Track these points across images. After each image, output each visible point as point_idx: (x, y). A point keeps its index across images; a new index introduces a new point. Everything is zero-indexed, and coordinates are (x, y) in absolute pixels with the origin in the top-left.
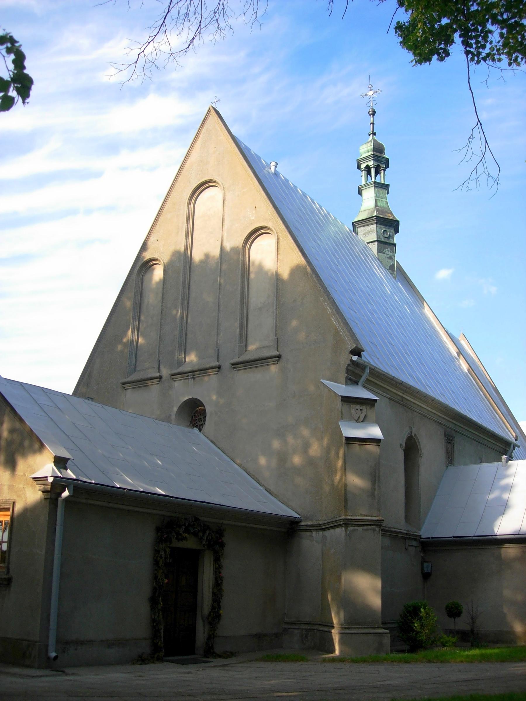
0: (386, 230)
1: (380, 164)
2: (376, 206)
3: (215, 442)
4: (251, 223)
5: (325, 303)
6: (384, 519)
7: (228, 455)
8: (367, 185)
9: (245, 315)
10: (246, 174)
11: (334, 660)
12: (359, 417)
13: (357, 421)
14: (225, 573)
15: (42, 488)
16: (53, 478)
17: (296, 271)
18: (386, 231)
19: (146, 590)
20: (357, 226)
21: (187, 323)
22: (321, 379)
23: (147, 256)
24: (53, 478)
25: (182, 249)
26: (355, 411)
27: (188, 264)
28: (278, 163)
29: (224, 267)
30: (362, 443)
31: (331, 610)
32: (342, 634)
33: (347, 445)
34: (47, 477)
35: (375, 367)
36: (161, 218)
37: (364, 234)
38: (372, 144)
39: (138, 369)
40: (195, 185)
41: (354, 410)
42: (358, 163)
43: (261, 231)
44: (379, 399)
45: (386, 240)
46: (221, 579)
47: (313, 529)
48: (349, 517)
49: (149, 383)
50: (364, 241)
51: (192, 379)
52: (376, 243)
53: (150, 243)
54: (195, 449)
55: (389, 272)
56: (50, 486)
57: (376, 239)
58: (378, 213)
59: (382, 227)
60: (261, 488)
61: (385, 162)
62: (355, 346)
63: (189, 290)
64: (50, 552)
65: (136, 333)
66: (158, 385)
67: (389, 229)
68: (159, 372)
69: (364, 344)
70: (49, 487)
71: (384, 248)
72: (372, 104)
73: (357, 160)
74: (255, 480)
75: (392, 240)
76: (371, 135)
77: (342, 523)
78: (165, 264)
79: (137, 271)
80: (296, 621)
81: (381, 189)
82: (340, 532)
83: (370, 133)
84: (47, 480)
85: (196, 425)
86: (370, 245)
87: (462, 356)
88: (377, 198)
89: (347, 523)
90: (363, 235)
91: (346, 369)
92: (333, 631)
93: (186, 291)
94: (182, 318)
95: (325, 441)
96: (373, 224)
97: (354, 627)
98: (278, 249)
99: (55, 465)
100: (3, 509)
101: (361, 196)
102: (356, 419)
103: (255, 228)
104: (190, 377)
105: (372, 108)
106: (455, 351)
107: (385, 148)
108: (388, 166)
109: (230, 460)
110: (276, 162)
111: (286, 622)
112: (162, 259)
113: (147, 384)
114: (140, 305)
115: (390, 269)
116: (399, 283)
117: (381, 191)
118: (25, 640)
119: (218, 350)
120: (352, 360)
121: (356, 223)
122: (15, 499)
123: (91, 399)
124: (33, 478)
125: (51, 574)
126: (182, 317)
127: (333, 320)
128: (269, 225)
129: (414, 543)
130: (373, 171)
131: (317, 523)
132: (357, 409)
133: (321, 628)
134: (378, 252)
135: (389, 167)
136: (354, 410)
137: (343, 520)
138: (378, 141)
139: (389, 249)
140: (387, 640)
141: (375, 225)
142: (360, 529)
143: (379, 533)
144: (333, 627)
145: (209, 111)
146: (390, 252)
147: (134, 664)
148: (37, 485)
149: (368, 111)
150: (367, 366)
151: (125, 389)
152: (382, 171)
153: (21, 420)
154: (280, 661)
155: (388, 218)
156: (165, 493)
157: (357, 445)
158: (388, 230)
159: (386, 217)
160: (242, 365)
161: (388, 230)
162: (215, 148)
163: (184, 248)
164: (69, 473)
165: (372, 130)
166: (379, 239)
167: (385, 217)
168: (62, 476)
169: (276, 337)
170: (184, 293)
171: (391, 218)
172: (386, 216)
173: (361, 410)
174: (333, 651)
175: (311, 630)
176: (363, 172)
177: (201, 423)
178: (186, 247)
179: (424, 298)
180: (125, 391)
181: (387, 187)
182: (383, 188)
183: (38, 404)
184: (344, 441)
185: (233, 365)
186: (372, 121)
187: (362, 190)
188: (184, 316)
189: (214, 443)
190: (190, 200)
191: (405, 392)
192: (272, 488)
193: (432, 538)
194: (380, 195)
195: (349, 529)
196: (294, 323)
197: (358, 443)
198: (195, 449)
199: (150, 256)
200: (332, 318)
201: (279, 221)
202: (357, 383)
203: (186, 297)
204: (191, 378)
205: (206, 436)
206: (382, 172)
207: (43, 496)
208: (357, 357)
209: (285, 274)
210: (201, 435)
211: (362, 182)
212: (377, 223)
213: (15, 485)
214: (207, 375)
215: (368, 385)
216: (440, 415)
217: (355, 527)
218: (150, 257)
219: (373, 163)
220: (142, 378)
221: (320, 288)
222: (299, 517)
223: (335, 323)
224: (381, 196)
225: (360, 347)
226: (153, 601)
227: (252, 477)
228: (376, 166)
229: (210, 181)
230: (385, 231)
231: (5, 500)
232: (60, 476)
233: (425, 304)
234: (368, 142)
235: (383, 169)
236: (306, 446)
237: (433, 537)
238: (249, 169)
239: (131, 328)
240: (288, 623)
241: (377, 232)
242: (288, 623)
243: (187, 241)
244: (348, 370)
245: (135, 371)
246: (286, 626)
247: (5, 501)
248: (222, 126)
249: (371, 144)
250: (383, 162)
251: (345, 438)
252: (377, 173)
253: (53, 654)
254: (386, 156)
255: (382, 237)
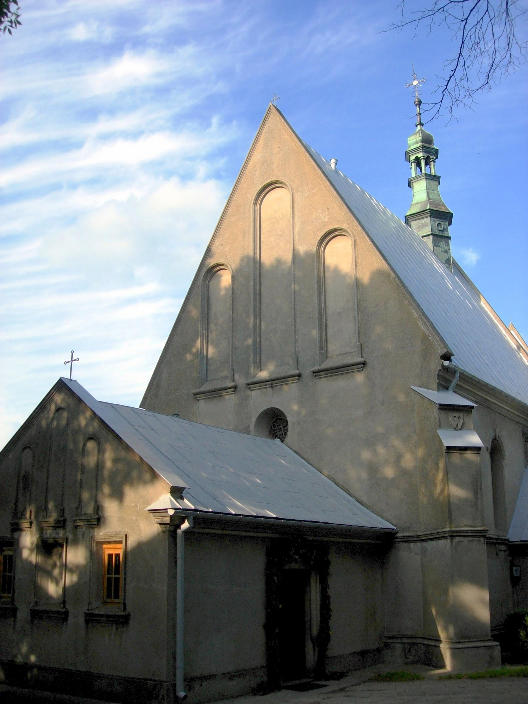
0: (440, 223)
1: (430, 155)
2: (428, 199)
3: (300, 452)
4: (325, 225)
5: (411, 307)
6: (489, 529)
7: (315, 466)
8: (417, 178)
9: (324, 320)
10: (315, 174)
11: (449, 677)
12: (457, 424)
13: (455, 429)
14: (330, 592)
15: (159, 520)
16: (173, 511)
17: (378, 274)
18: (440, 224)
19: (260, 617)
20: (410, 220)
21: (260, 331)
22: (411, 385)
23: (211, 262)
24: (173, 511)
25: (251, 253)
26: (453, 419)
27: (258, 269)
28: (338, 160)
29: (299, 274)
30: (463, 452)
31: (437, 623)
32: (453, 649)
33: (448, 455)
34: (166, 509)
35: (464, 371)
36: (225, 222)
37: (418, 228)
38: (421, 135)
39: (209, 378)
40: (260, 187)
41: (451, 417)
42: (407, 155)
43: (335, 233)
44: (476, 405)
45: (440, 234)
46: (328, 597)
47: (411, 541)
48: (454, 529)
49: (224, 393)
50: (418, 235)
51: (271, 388)
52: (431, 237)
53: (213, 248)
54: (284, 462)
55: (445, 265)
56: (169, 519)
57: (431, 233)
58: (431, 206)
59: (436, 220)
60: (352, 499)
61: (434, 153)
62: (446, 351)
63: (260, 295)
64: (172, 586)
65: (205, 342)
66: (234, 395)
67: (443, 222)
68: (233, 381)
69: (454, 350)
70: (167, 520)
71: (439, 242)
72: (417, 94)
73: (406, 152)
74: (345, 492)
75: (447, 233)
76: (419, 126)
77: (447, 535)
78: (233, 269)
79: (203, 278)
80: (397, 635)
81: (433, 181)
82: (445, 544)
83: (417, 124)
84: (167, 512)
85: (276, 435)
86: (425, 239)
87: (522, 350)
88: (429, 191)
89: (453, 535)
90: (417, 228)
91: (437, 375)
92: (442, 645)
93: (258, 297)
94: (255, 325)
95: (420, 452)
96: (427, 217)
97: (464, 641)
98: (355, 251)
99: (171, 495)
100: (113, 541)
101: (411, 189)
102: (455, 427)
103: (329, 230)
104: (268, 386)
105: (418, 98)
106: (515, 344)
107: (434, 139)
108: (437, 158)
109: (316, 471)
110: (336, 159)
111: (386, 636)
112: (229, 264)
113: (221, 394)
114: (208, 312)
115: (446, 263)
116: (455, 277)
117: (432, 182)
118: (151, 680)
119: (297, 357)
120: (443, 366)
121: (409, 216)
122: (127, 531)
123: (178, 415)
124: (149, 510)
125: (175, 609)
126: (255, 324)
127: (420, 324)
128: (344, 226)
129: (503, 547)
130: (423, 163)
131: (415, 534)
132: (455, 417)
133: (426, 642)
134: (433, 246)
135: (438, 158)
136: (451, 418)
137: (448, 532)
138: (426, 132)
139: (444, 242)
140: (497, 652)
141: (429, 218)
142: (466, 540)
143: (484, 543)
144: (440, 641)
145: (270, 109)
146: (446, 245)
147: (255, 695)
148: (153, 517)
149: (414, 101)
150: (457, 370)
151: (198, 400)
152: (432, 162)
153: (128, 448)
154: (395, 681)
155: (442, 210)
156: (276, 515)
157: (458, 454)
158: (442, 223)
159: (440, 210)
160: (324, 372)
161: (442, 223)
162: (279, 147)
163: (252, 252)
164: (186, 503)
165: (419, 120)
166: (433, 233)
167: (438, 209)
168: (181, 508)
169: (360, 343)
170: (255, 299)
171: (444, 210)
172: (439, 208)
173: (458, 417)
174: (443, 666)
175: (414, 644)
176: (413, 164)
177: (282, 433)
178: (255, 251)
179: (480, 291)
180: (197, 402)
181: (438, 179)
182: (434, 180)
183: (133, 427)
184: (445, 451)
185: (314, 372)
186: (418, 111)
187: (412, 183)
188: (257, 323)
189: (299, 453)
190: (255, 202)
191: (488, 393)
192: (364, 499)
193: (521, 541)
194: (431, 187)
195: (454, 540)
196: (379, 329)
197: (459, 452)
198: (284, 462)
199: (216, 261)
200: (419, 322)
201: (354, 223)
202: (447, 388)
203: (258, 303)
204: (269, 387)
205: (288, 447)
206: (432, 163)
207: (161, 528)
208: (449, 362)
209: (365, 277)
210: (283, 445)
211: (411, 175)
212: (430, 216)
213: (125, 516)
214: (286, 384)
215: (459, 390)
216: (518, 414)
217: (461, 539)
218: (216, 262)
219: (423, 155)
220: (216, 387)
221: (404, 291)
222: (395, 528)
223: (422, 327)
224: (432, 188)
225: (450, 352)
226: (268, 627)
227: (341, 488)
228: (426, 158)
229: (275, 182)
230: (439, 224)
231: (115, 532)
232: (180, 508)
233: (481, 297)
234: (416, 133)
235: (433, 160)
236: (399, 457)
237: (522, 540)
238: (318, 169)
239: (200, 338)
240: (390, 638)
241: (431, 225)
242: (390, 638)
243: (255, 245)
244: (439, 375)
245: (207, 380)
246: (387, 641)
247: (116, 533)
248: (284, 124)
249: (419, 134)
250: (432, 153)
251: (446, 448)
252: (427, 164)
253: (182, 694)
254: (435, 147)
255: (437, 231)
